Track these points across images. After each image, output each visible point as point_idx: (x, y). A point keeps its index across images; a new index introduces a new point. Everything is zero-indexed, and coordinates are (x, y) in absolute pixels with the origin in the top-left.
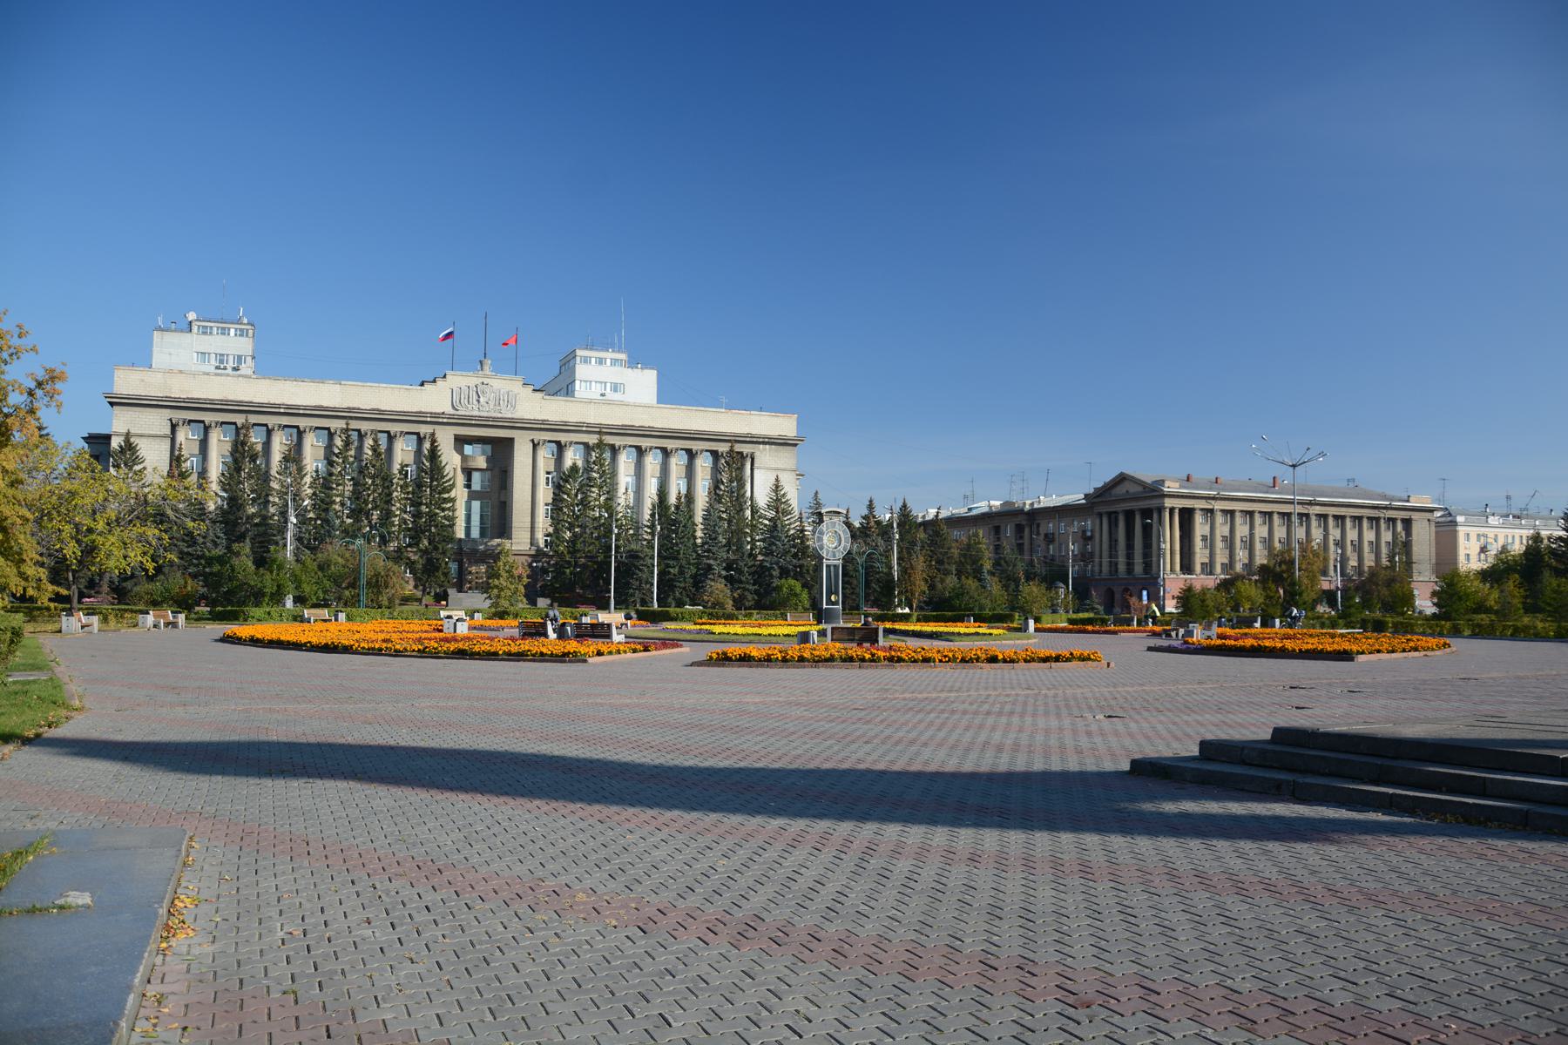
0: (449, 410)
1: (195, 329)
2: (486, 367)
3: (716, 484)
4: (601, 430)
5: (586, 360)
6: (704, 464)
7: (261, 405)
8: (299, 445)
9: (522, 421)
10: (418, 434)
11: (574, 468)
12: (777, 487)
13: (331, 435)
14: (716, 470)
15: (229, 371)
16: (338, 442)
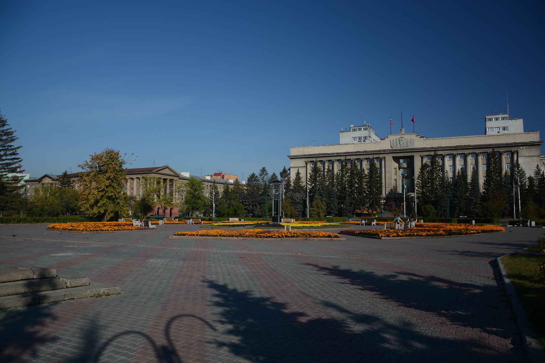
0: (390, 148)
1: (351, 130)
2: (403, 132)
4: (435, 150)
5: (490, 120)
6: (482, 160)
7: (329, 154)
9: (415, 149)
10: (511, 151)
12: (298, 174)
14: (488, 160)
15: (362, 142)
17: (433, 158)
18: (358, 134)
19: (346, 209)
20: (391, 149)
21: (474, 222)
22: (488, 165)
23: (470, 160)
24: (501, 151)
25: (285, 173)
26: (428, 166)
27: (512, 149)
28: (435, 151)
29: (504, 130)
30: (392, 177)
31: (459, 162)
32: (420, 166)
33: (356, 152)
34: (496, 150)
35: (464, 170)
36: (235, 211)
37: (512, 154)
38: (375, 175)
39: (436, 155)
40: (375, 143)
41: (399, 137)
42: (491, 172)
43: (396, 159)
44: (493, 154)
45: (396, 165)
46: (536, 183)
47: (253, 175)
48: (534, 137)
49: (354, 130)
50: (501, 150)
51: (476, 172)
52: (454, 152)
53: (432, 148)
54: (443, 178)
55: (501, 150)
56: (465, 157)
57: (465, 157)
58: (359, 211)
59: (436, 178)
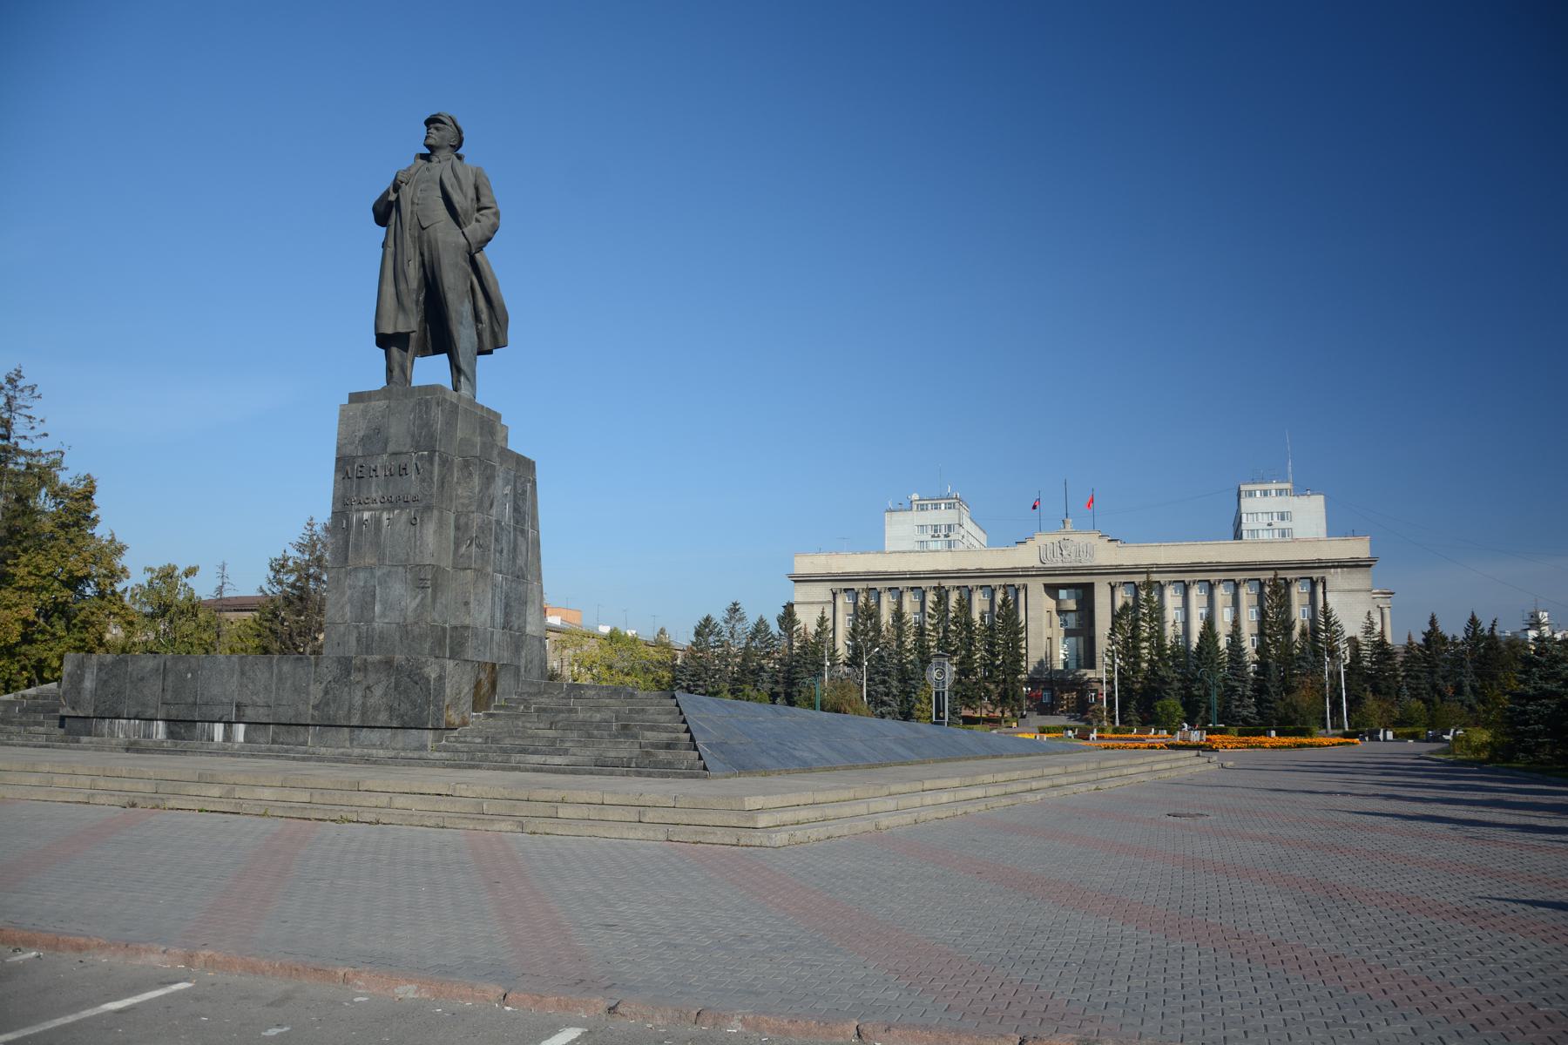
2: (1068, 527)
3: (1263, 614)
4: (1148, 570)
5: (1251, 494)
6: (1247, 595)
7: (892, 573)
8: (900, 604)
9: (1098, 567)
11: (1125, 607)
13: (993, 591)
14: (1261, 596)
18: (931, 517)
23: (1222, 595)
25: (788, 617)
27: (1315, 572)
33: (958, 571)
37: (1313, 584)
38: (1007, 624)
40: (974, 550)
41: (1060, 538)
43: (1052, 590)
44: (1274, 586)
45: (1052, 603)
46: (1366, 651)
47: (708, 619)
48: (1358, 548)
49: (922, 508)
50: (1290, 575)
52: (1186, 575)
55: (1290, 575)
58: (966, 712)
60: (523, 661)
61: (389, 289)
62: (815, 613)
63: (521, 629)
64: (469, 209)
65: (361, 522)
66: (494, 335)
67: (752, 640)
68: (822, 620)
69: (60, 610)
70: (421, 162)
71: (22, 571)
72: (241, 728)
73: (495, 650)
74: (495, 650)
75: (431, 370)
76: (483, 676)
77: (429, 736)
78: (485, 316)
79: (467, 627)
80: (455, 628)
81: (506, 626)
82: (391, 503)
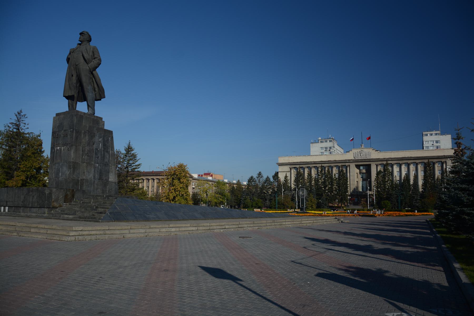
0: (353, 158)
2: (363, 147)
4: (387, 160)
5: (426, 135)
6: (420, 167)
7: (308, 162)
8: (311, 171)
9: (372, 159)
13: (339, 167)
16: (320, 169)
17: (385, 166)
18: (324, 145)
19: (323, 203)
20: (354, 159)
21: (416, 211)
22: (425, 171)
23: (412, 167)
24: (434, 161)
25: (276, 176)
26: (382, 172)
28: (387, 161)
29: (437, 143)
30: (355, 180)
31: (404, 168)
32: (376, 172)
33: (329, 161)
34: (430, 160)
35: (408, 175)
36: (257, 204)
37: (442, 164)
38: (343, 177)
39: (387, 164)
40: (339, 154)
41: (360, 150)
42: (427, 177)
43: (358, 167)
45: (358, 171)
47: (252, 177)
49: (322, 142)
50: (434, 161)
51: (416, 177)
52: (400, 161)
53: (384, 159)
54: (392, 181)
55: (434, 161)
56: (408, 165)
57: (408, 165)
58: (331, 205)
59: (387, 181)
60: (108, 189)
61: (68, 83)
62: (284, 174)
63: (107, 180)
64: (94, 60)
65: (57, 150)
66: (100, 95)
67: (265, 183)
68: (286, 177)
69: (33, 177)
70: (79, 46)
71: (22, 166)
72: (7, 208)
73: (96, 186)
74: (96, 186)
75: (82, 107)
76: (68, 193)
77: (46, 210)
78: (97, 89)
79: (84, 179)
80: (81, 180)
81: (100, 179)
82: (64, 145)
